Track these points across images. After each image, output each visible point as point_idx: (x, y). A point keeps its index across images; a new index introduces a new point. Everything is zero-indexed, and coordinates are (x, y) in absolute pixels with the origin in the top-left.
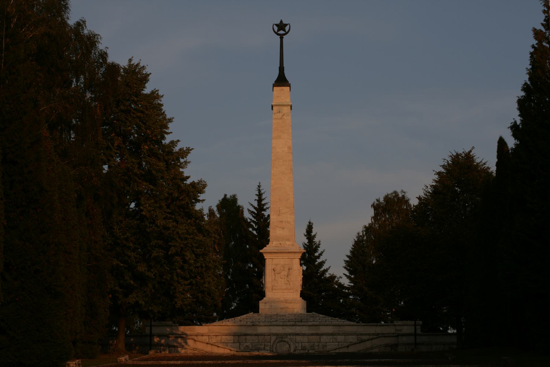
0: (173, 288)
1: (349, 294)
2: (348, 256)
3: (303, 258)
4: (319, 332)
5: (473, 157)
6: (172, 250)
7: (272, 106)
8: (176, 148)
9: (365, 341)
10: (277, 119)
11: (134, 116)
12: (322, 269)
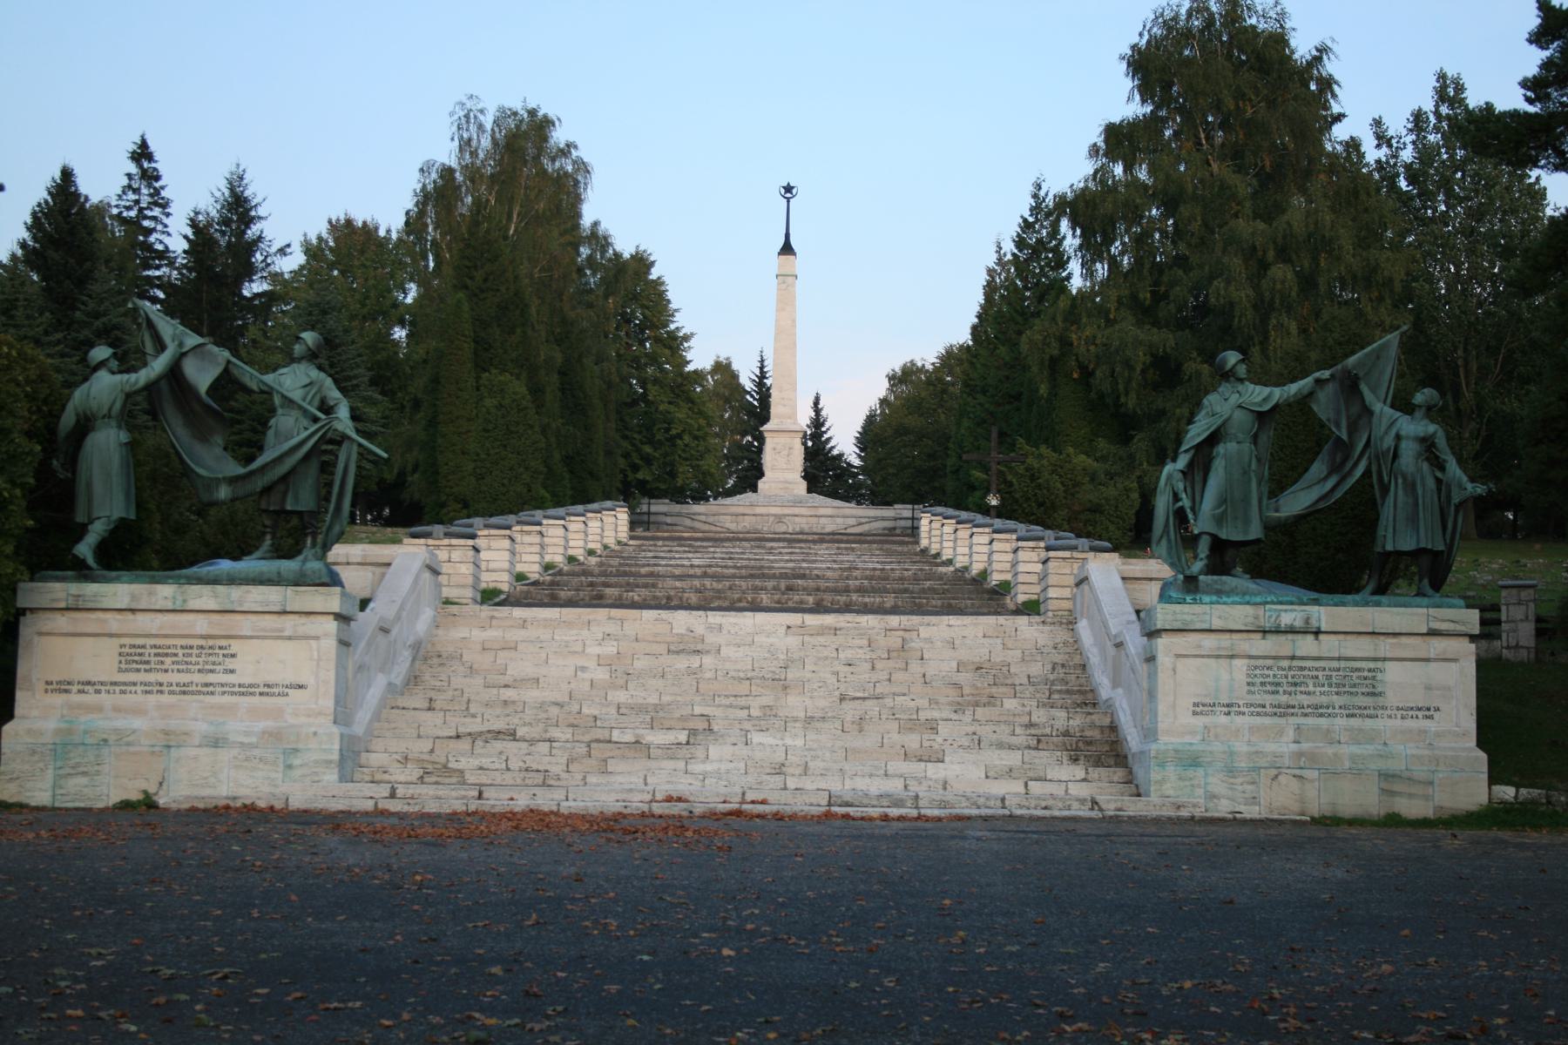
1: (858, 474)
12: (829, 446)
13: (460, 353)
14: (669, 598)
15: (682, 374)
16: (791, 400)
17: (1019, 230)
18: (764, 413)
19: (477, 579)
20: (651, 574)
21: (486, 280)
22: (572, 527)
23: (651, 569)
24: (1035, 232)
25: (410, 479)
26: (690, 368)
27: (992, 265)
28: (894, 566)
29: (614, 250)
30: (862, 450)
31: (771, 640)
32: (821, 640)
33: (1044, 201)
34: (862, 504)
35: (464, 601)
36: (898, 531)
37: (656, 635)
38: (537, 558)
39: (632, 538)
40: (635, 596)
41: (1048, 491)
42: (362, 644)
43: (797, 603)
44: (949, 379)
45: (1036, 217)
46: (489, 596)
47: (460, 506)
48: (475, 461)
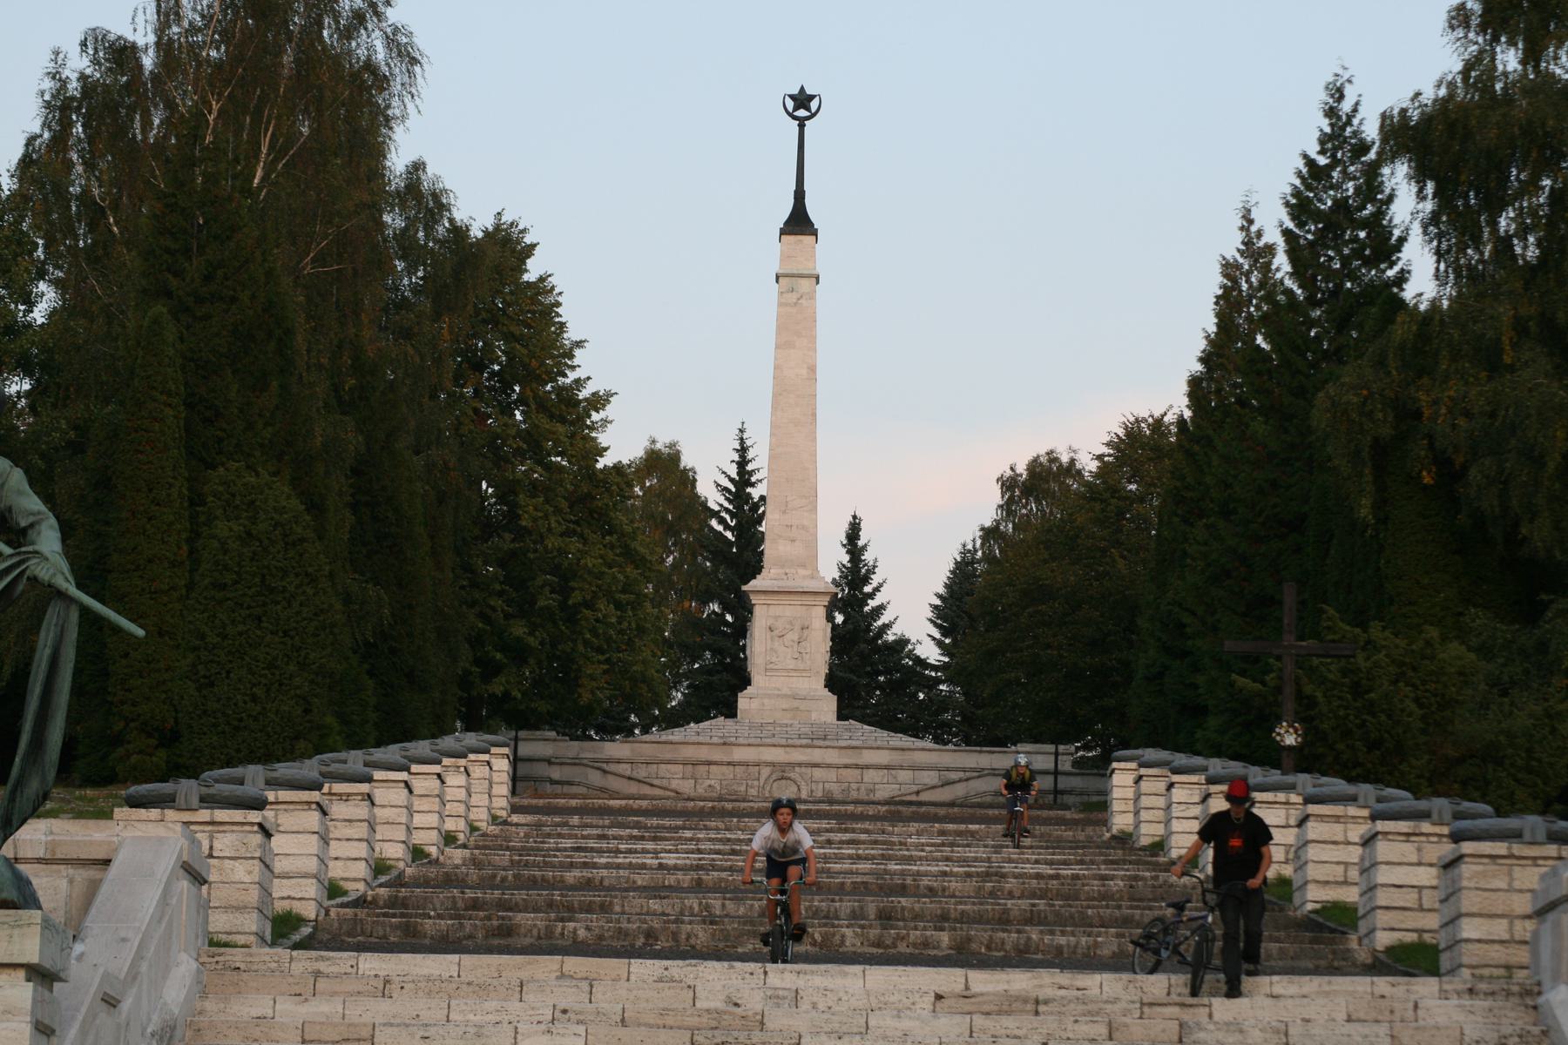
0: (575, 667)
1: (938, 681)
2: (939, 596)
3: (834, 605)
4: (860, 762)
6: (576, 597)
9: (954, 783)
12: (879, 623)
13: (157, 427)
14: (650, 935)
15: (591, 474)
16: (804, 528)
17: (1297, 182)
18: (748, 554)
19: (266, 891)
20: (588, 884)
21: (208, 278)
22: (419, 785)
23: (587, 873)
24: (1332, 187)
25: (1541, 624)
28: (1076, 870)
29: (451, 220)
30: (945, 632)
31: (906, 1024)
32: (1010, 1023)
33: (1349, 122)
34: (945, 743)
35: (241, 939)
37: (664, 1012)
38: (361, 850)
39: (515, 809)
40: (579, 928)
41: (1390, 717)
42: (73, 1032)
43: (915, 945)
44: (1133, 487)
45: (1333, 156)
46: (283, 928)
47: (153, 742)
48: (195, 649)
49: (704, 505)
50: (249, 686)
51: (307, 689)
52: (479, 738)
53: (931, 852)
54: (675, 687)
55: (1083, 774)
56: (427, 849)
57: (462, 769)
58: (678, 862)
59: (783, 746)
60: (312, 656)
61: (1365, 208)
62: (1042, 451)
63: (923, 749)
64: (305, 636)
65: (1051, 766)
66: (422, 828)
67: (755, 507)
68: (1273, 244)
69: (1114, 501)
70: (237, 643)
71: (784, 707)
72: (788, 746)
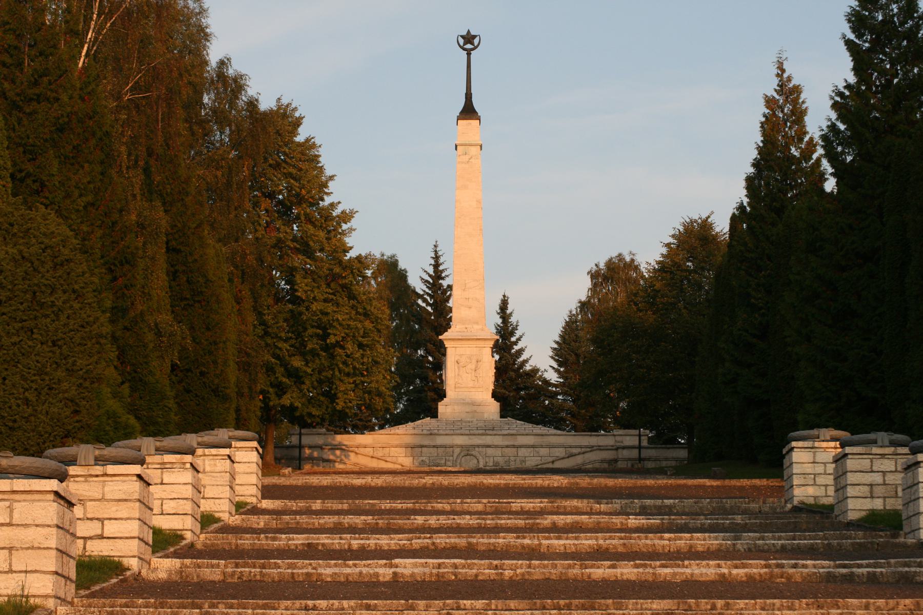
1: (557, 394)
2: (557, 343)
4: (516, 443)
5: (712, 224)
6: (332, 340)
7: (456, 146)
8: (336, 211)
10: (462, 163)
11: (285, 171)
12: (521, 359)
26: (352, 254)
27: (771, 93)
36: (621, 465)
49: (414, 292)
50: (21, 390)
51: (74, 392)
52: (231, 434)
53: (669, 540)
54: (399, 401)
55: (656, 448)
56: (126, 562)
57: (188, 466)
58: (416, 571)
59: (467, 435)
60: (79, 362)
61: (907, 23)
62: (614, 254)
63: (555, 435)
64: (72, 345)
65: (637, 443)
66: (121, 538)
67: (445, 292)
68: (799, 85)
69: (678, 272)
70: (11, 352)
71: (468, 410)
72: (471, 435)
